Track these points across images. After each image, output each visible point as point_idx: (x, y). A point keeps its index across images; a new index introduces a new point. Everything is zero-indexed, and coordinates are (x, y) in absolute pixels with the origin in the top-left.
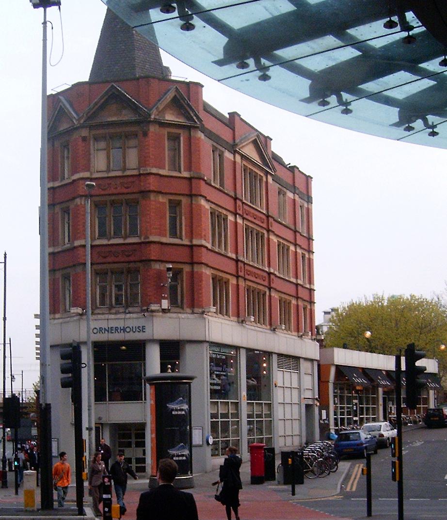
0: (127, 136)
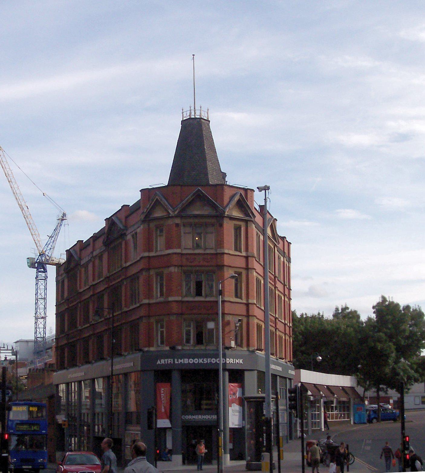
0: (206, 225)
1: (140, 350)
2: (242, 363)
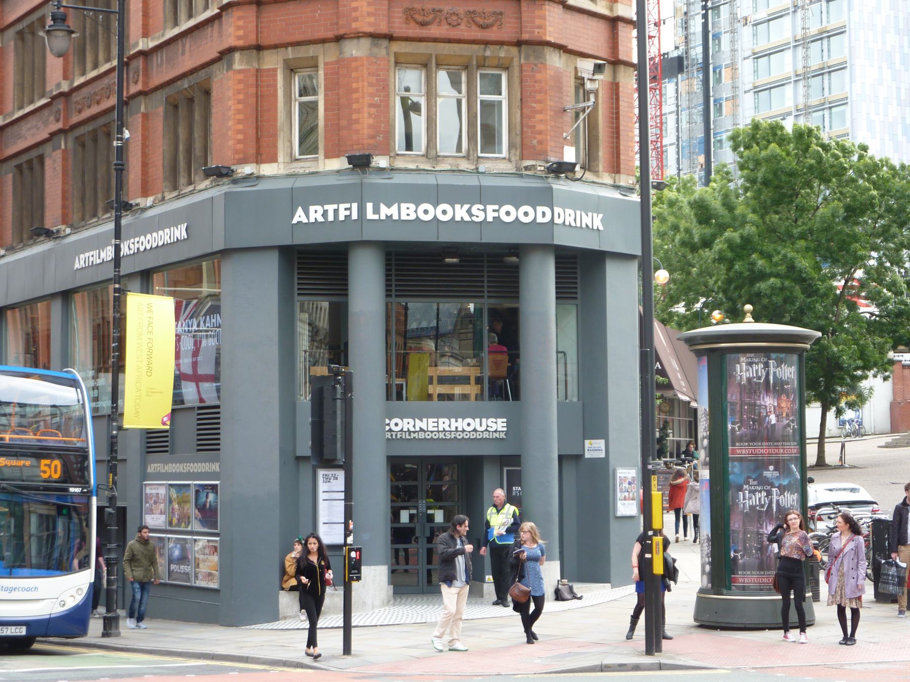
1: (221, 173)
2: (601, 228)
